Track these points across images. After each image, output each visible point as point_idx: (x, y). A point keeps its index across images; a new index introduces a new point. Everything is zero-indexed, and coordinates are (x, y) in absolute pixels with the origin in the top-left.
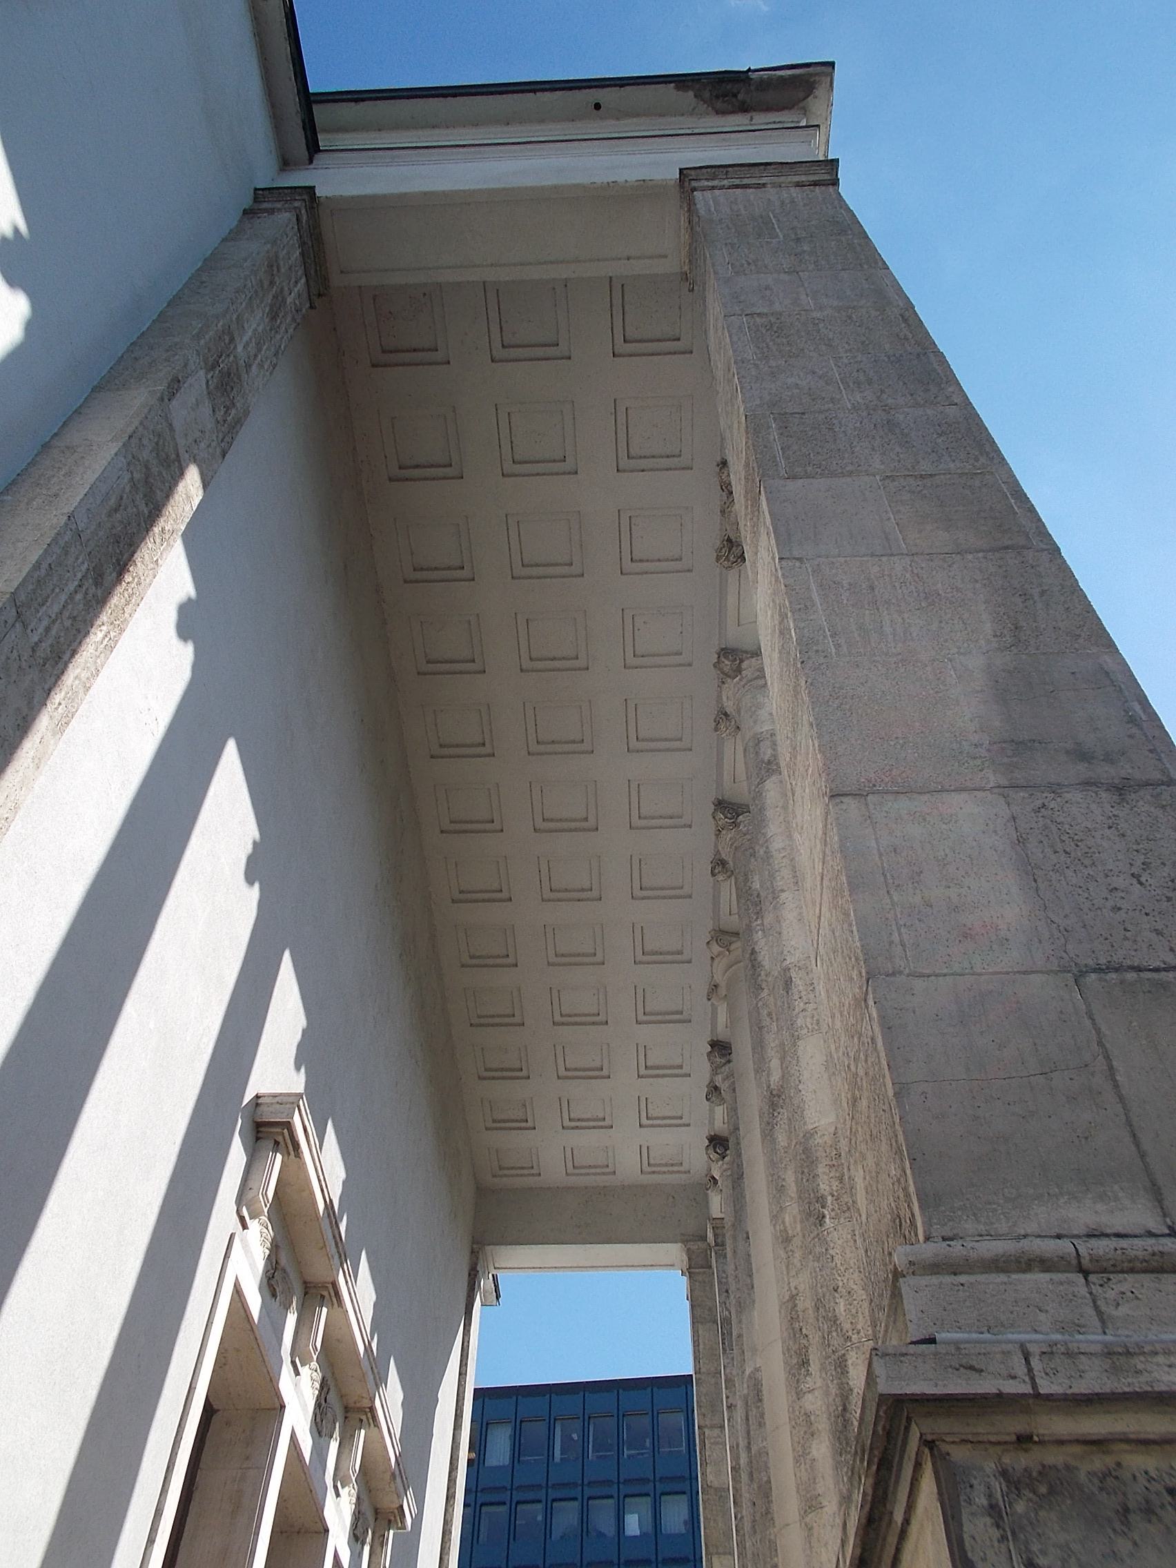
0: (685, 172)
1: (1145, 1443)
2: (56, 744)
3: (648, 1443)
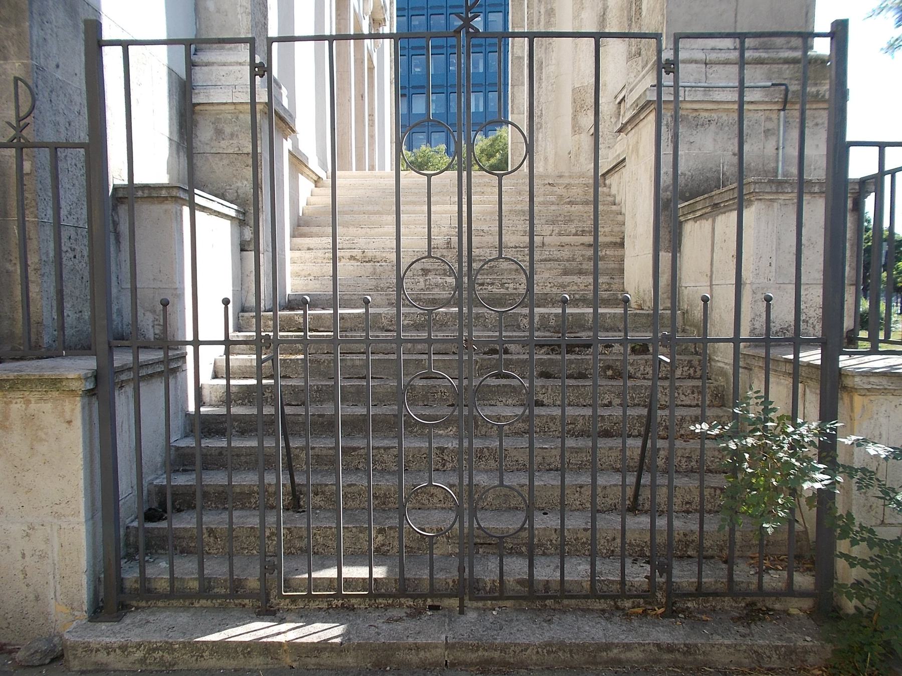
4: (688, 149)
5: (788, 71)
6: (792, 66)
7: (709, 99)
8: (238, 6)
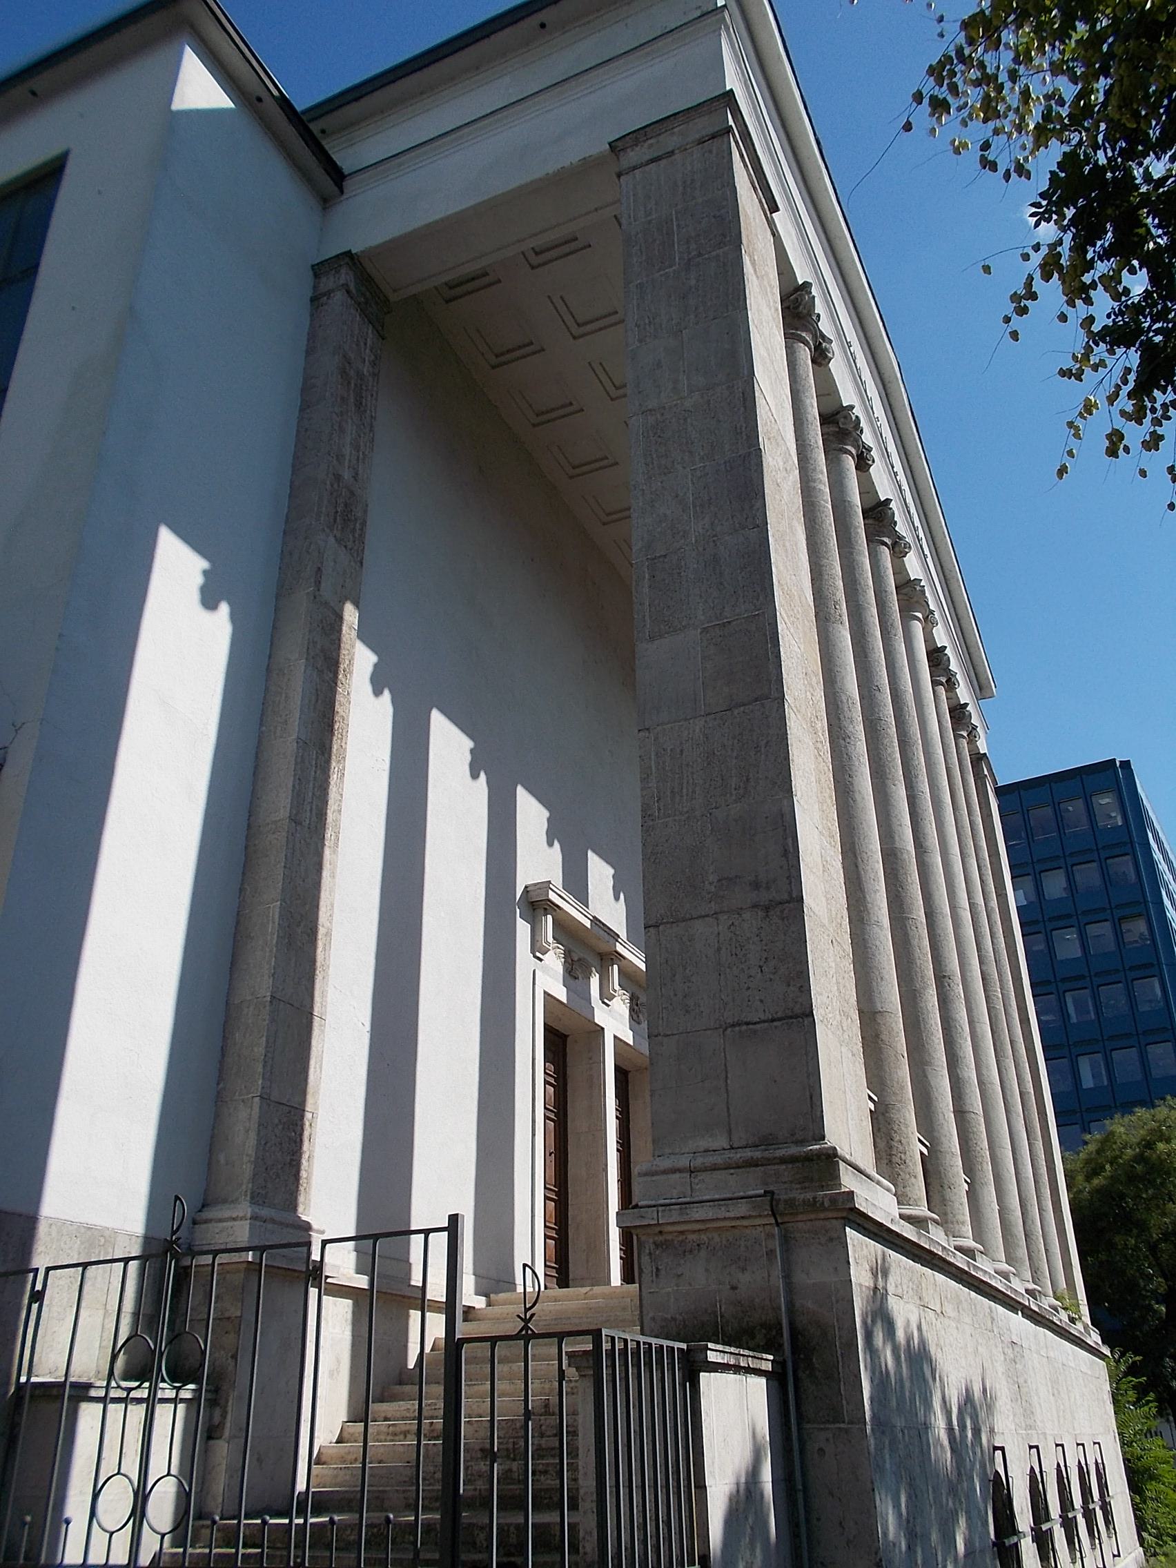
0: (613, 144)
1: (694, 1232)
2: (337, 856)
3: (1023, 835)
4: (677, 1285)
5: (786, 1173)
6: (790, 1166)
7: (686, 1218)
8: (244, 1156)
